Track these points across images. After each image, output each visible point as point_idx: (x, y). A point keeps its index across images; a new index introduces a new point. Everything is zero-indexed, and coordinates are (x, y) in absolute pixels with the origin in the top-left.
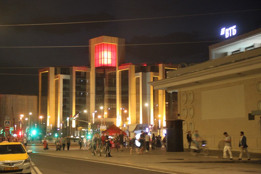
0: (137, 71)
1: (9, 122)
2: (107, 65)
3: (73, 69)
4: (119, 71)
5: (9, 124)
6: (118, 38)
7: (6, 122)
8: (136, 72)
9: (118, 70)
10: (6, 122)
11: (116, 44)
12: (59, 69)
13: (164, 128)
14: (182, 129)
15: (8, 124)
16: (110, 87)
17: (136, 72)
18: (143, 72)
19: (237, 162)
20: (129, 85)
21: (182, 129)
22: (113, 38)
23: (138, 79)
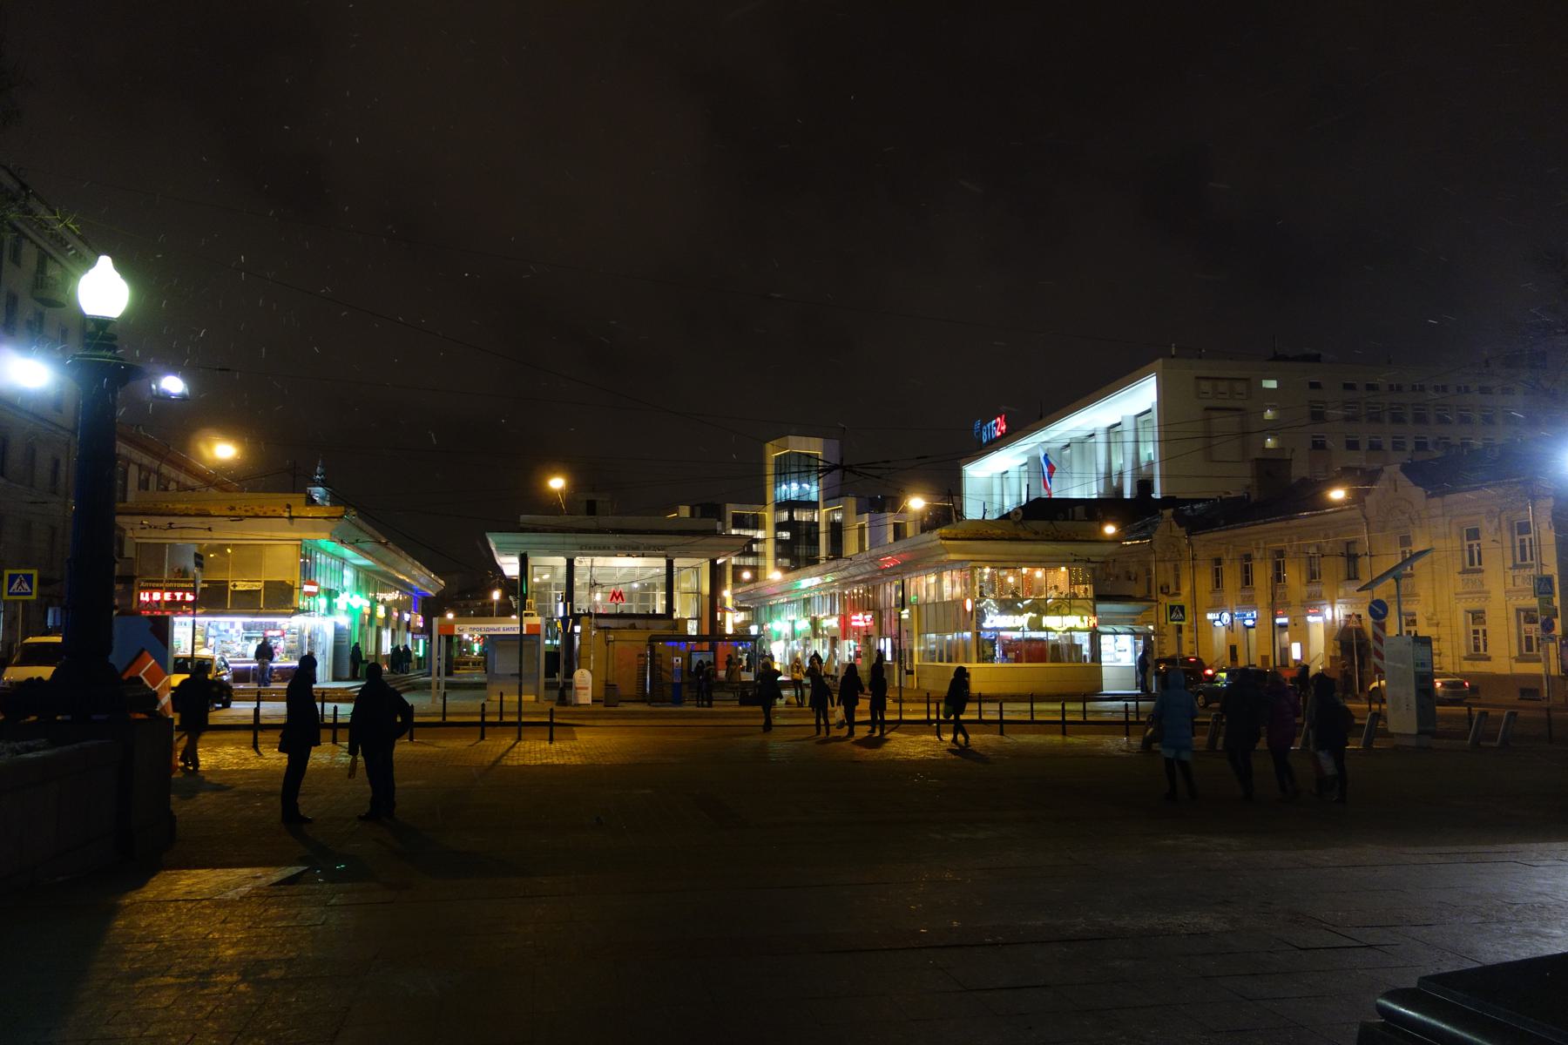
0: (860, 512)
1: (29, 578)
2: (829, 534)
3: (727, 509)
4: (824, 510)
5: (31, 587)
6: (822, 440)
7: (12, 578)
8: (858, 514)
9: (824, 508)
10: (12, 578)
11: (820, 453)
12: (698, 509)
13: (901, 717)
14: (35, 678)
15: (26, 586)
16: (808, 547)
17: (858, 514)
18: (296, 672)
19: (37, 279)
20: (843, 542)
21: (35, 678)
22: (811, 439)
23: (862, 528)
